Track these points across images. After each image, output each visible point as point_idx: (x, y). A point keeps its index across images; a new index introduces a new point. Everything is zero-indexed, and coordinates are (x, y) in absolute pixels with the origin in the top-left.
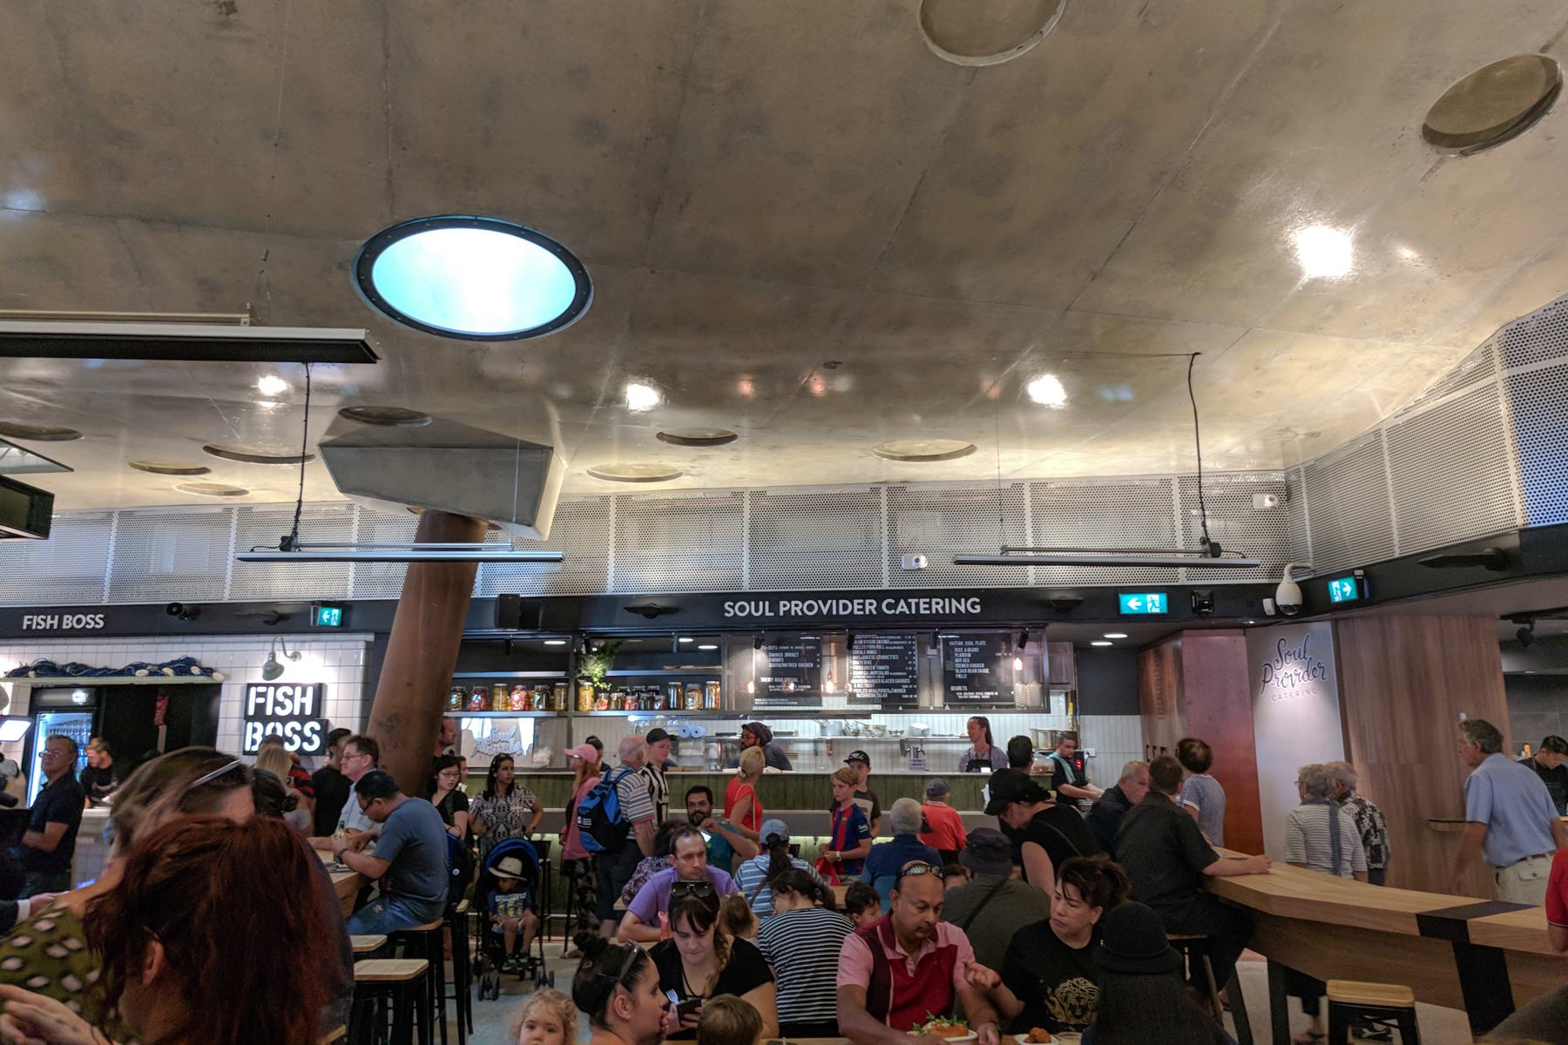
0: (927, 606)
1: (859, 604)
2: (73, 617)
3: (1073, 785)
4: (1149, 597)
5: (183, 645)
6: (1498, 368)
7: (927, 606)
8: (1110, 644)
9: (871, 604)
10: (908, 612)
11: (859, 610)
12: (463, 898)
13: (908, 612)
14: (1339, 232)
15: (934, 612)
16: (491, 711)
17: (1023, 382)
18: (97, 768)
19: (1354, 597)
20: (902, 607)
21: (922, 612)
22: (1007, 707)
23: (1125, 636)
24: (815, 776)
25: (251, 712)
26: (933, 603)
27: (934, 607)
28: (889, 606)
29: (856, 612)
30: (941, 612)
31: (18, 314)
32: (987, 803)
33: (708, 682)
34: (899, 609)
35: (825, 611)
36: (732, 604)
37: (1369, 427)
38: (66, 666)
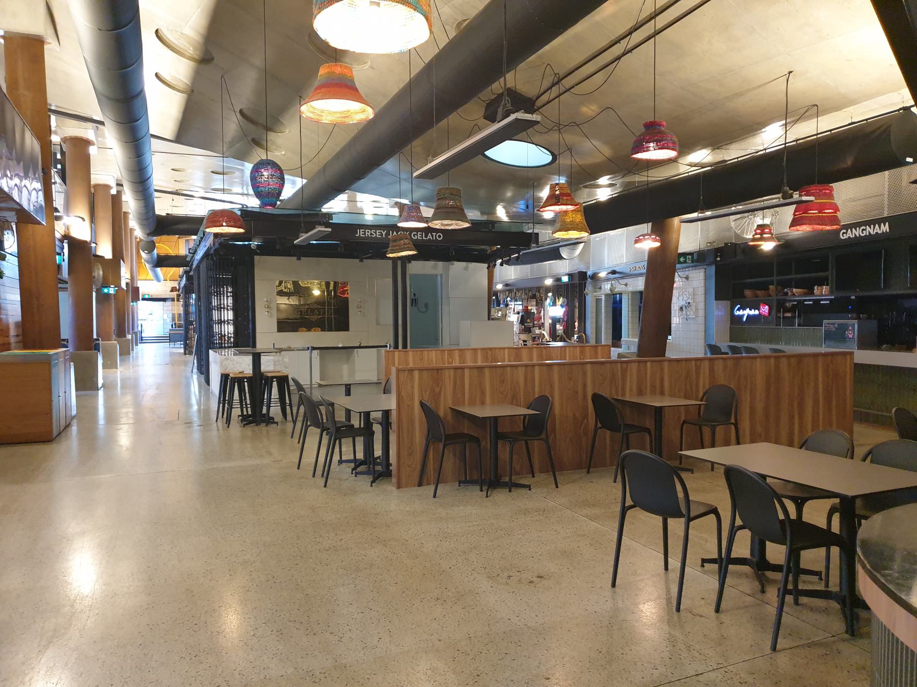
1: (362, 231)
8: (828, 302)
10: (432, 239)
11: (362, 234)
13: (432, 239)
14: (207, 211)
15: (367, 236)
18: (448, 171)
21: (361, 235)
23: (415, 253)
24: (462, 163)
27: (367, 233)
29: (378, 236)
30: (370, 236)
31: (768, 199)
32: (44, 206)
34: (428, 237)
35: (395, 233)
38: (207, 274)
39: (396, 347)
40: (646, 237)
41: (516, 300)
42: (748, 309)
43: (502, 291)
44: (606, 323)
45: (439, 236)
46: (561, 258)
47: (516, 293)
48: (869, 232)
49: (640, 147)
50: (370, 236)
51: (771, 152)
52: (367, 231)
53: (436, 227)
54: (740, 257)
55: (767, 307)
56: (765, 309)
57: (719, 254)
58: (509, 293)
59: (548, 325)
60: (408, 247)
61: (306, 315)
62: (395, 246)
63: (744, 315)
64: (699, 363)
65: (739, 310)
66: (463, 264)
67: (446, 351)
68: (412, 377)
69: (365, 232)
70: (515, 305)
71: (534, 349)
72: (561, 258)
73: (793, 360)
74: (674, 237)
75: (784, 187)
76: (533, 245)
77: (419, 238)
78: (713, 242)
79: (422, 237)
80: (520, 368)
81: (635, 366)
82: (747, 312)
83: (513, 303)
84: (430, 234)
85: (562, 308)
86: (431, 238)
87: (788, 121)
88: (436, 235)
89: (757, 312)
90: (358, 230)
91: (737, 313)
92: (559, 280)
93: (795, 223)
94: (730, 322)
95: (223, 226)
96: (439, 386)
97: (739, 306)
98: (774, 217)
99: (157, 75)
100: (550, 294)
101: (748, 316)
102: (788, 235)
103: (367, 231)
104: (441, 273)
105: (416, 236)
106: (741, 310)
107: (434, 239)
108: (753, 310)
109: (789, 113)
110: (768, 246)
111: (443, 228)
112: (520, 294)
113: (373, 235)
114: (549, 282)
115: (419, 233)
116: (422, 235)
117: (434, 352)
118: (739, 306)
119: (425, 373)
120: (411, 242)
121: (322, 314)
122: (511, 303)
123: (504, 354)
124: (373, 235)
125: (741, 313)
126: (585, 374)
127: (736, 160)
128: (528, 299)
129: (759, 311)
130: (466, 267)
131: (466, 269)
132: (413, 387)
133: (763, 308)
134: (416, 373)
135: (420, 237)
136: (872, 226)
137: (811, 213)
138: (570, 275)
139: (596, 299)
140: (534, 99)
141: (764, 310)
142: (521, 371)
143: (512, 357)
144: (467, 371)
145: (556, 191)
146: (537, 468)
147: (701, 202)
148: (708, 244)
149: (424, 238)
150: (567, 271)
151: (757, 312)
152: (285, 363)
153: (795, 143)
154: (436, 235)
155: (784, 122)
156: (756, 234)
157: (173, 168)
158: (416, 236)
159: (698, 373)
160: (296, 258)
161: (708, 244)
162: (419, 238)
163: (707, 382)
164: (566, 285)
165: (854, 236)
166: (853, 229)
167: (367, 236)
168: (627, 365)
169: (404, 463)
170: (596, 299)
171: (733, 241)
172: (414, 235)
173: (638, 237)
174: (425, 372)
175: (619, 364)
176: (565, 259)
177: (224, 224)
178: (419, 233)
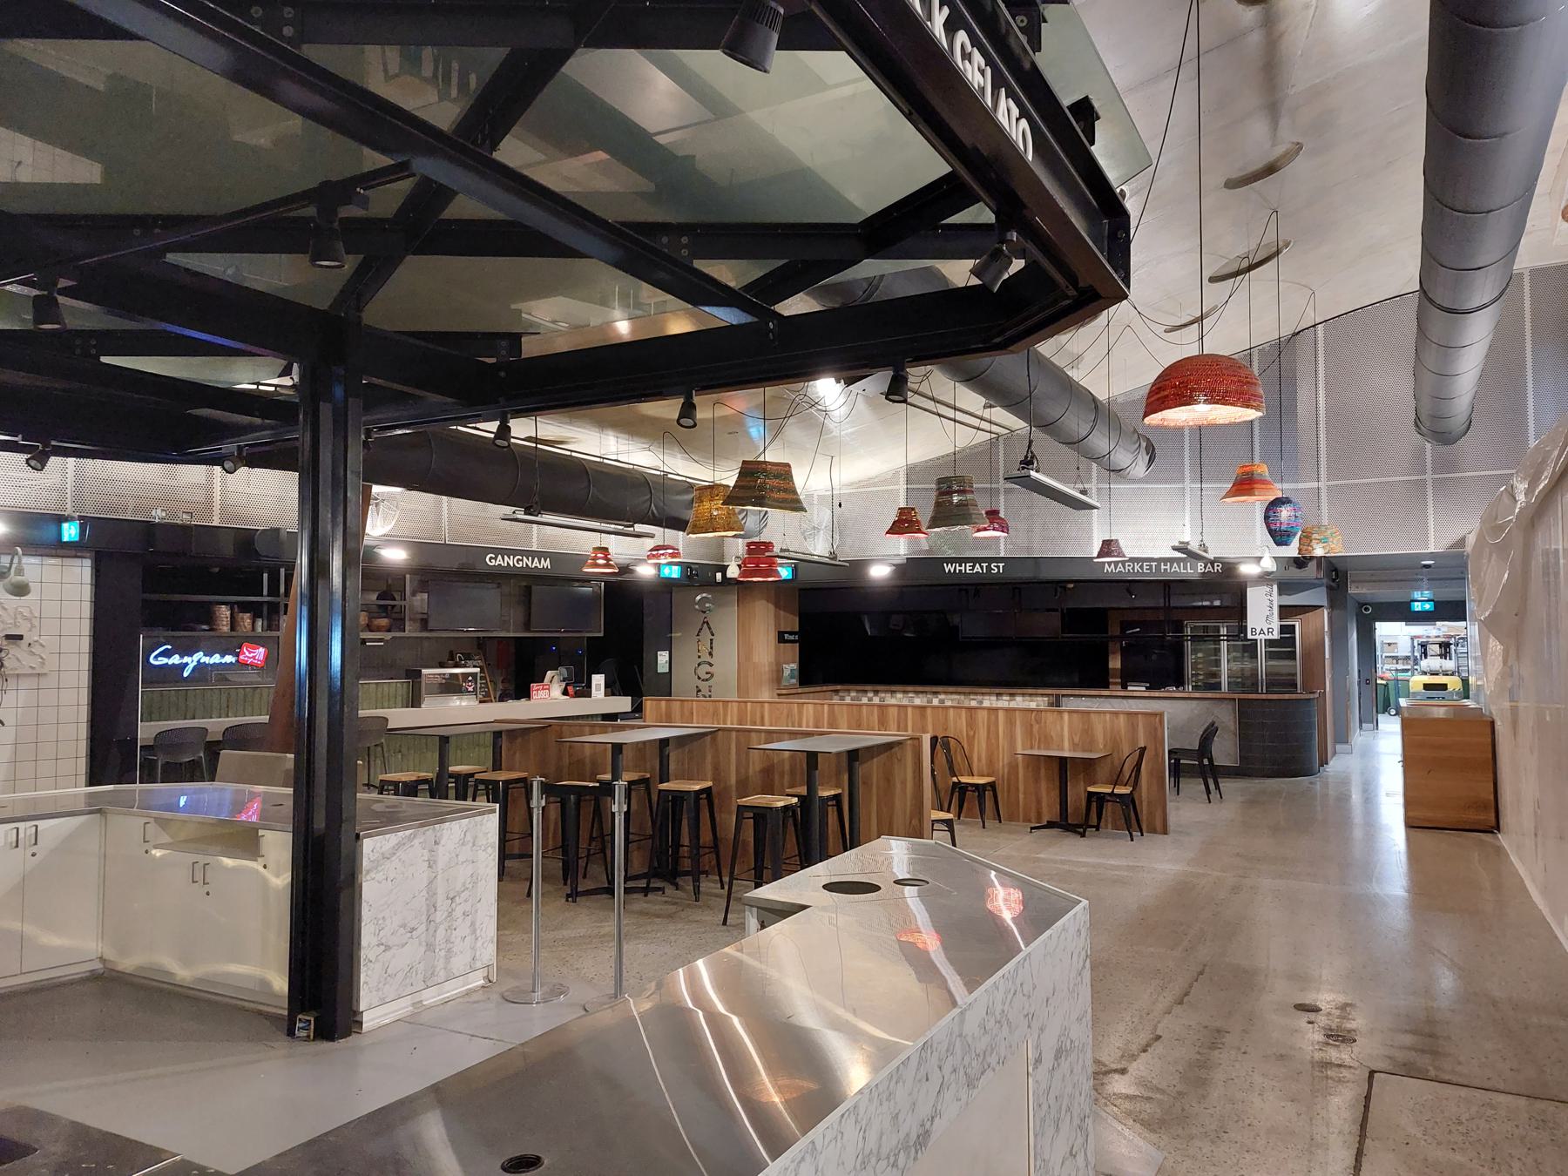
5: (76, 560)
6: (1429, 471)
9: (1218, 566)
16: (624, 893)
19: (77, 539)
20: (499, 561)
21: (968, 571)
22: (784, 501)
25: (988, 794)
27: (1216, 568)
33: (492, 436)
44: (1352, 647)
48: (527, 564)
51: (577, 458)
68: (1062, 718)
105: (520, 562)
106: (177, 656)
118: (169, 647)
127: (631, 467)
132: (1062, 728)
133: (250, 652)
135: (1147, 569)
136: (530, 558)
143: (1076, 735)
146: (1531, 724)
158: (520, 562)
165: (506, 565)
166: (536, 559)
174: (1075, 715)
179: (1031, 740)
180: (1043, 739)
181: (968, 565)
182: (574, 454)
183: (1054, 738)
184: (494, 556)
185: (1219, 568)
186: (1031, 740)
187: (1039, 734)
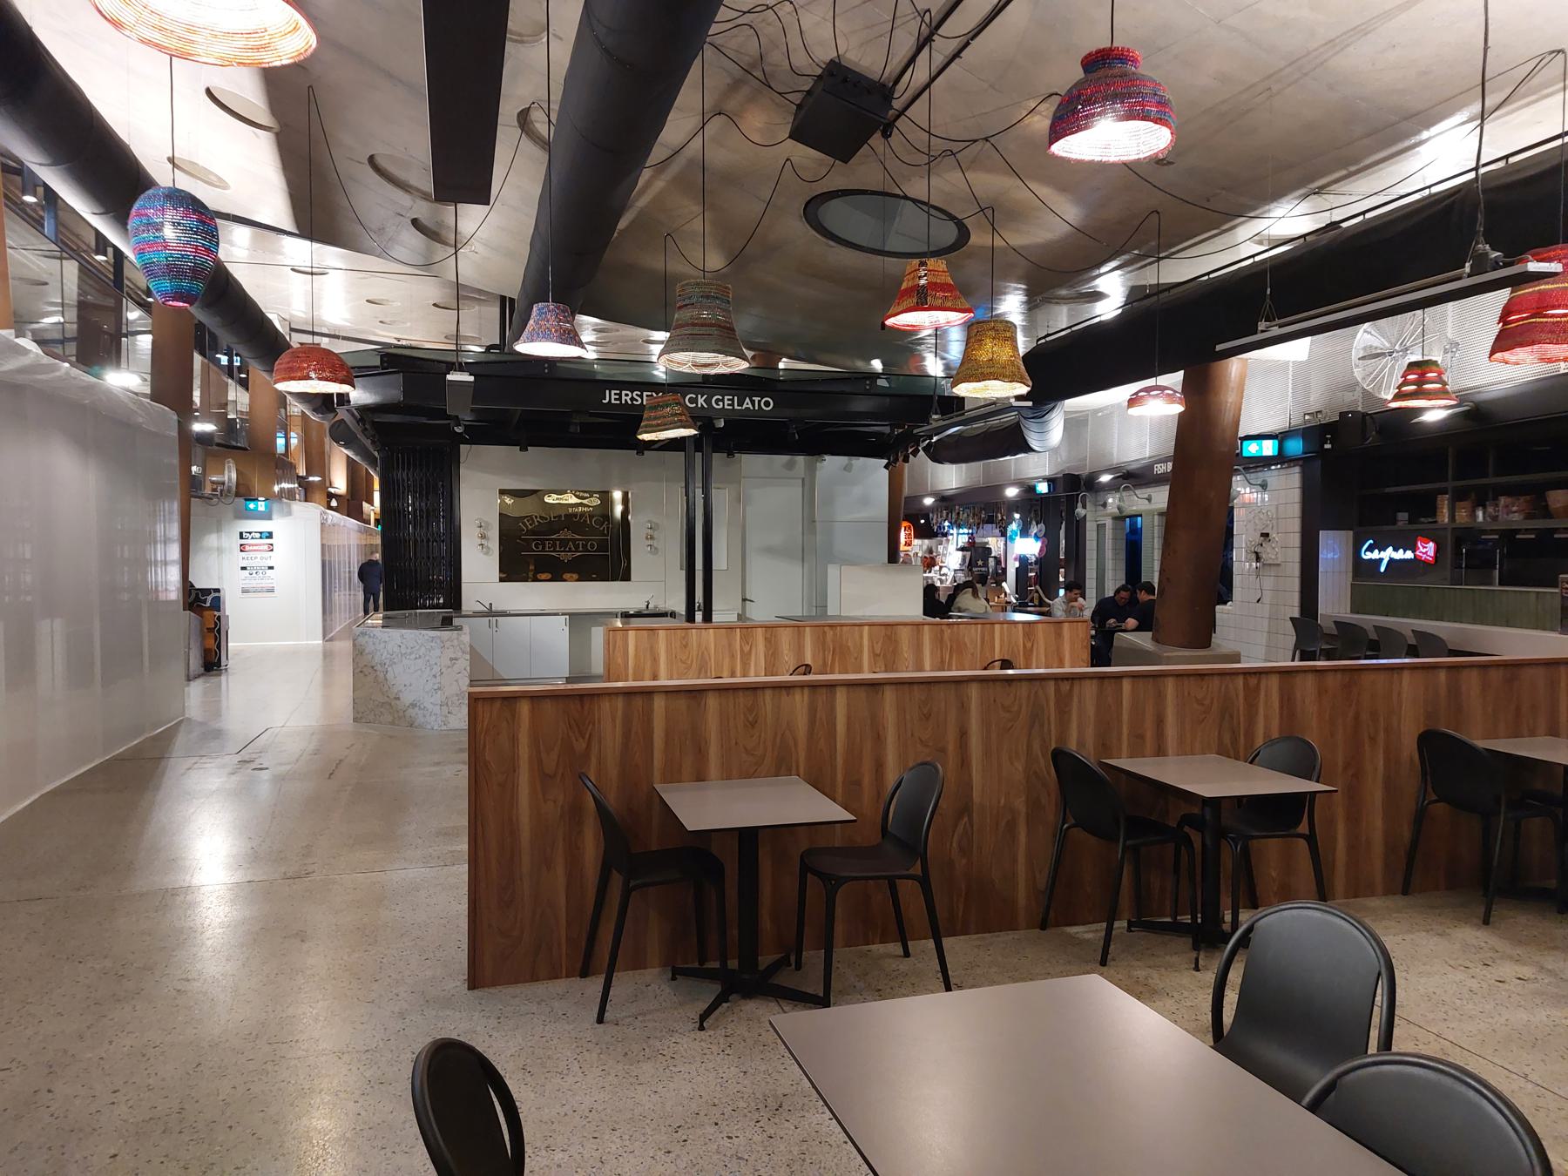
0: (617, 397)
1: (615, 394)
2: (762, 399)
3: (931, 671)
4: (324, 338)
7: (617, 397)
10: (752, 408)
11: (616, 399)
12: (1560, 261)
13: (752, 408)
15: (623, 402)
17: (1005, 294)
21: (613, 401)
26: (623, 395)
27: (624, 398)
28: (691, 400)
30: (630, 402)
34: (745, 406)
36: (639, 393)
37: (1110, 463)
39: (690, 617)
40: (1152, 393)
41: (959, 527)
42: (1391, 548)
43: (932, 509)
45: (767, 404)
46: (1027, 449)
47: (958, 514)
49: (1068, 119)
50: (630, 402)
52: (624, 392)
53: (681, 369)
54: (1372, 438)
55: (1431, 545)
56: (1428, 550)
57: (1329, 436)
58: (947, 514)
59: (1014, 571)
60: (681, 421)
61: (551, 551)
62: (655, 418)
63: (1381, 560)
64: (1253, 681)
65: (1370, 549)
66: (841, 460)
67: (738, 630)
69: (620, 395)
70: (958, 534)
71: (926, 627)
72: (1027, 449)
73: (1496, 676)
74: (1230, 400)
75: (1477, 243)
76: (935, 417)
77: (726, 407)
78: (1317, 412)
79: (733, 405)
80: (798, 692)
81: (1090, 689)
82: (1388, 554)
83: (954, 531)
84: (748, 400)
85: (1037, 541)
86: (750, 406)
87: (1490, 102)
88: (759, 402)
89: (1409, 555)
90: (607, 392)
91: (1368, 556)
92: (1032, 489)
93: (1505, 341)
94: (1351, 574)
95: (311, 378)
96: (583, 738)
97: (1371, 541)
98: (1449, 355)
99: (209, 92)
100: (1017, 516)
101: (1391, 560)
102: (1479, 392)
103: (624, 392)
104: (803, 476)
105: (721, 403)
107: (757, 408)
108: (1401, 551)
109: (1488, 80)
110: (1435, 413)
111: (697, 371)
112: (965, 515)
113: (637, 401)
114: (1012, 492)
115: (726, 398)
116: (733, 400)
117: (711, 631)
118: (1371, 541)
119: (548, 706)
120: (686, 413)
121: (581, 549)
122: (951, 531)
123: (861, 637)
124: (637, 401)
125: (1375, 555)
126: (963, 708)
127: (1360, 218)
128: (979, 524)
129: (1414, 551)
130: (847, 465)
131: (847, 468)
132: (514, 740)
133: (1424, 547)
134: (524, 708)
137: (1553, 316)
138: (1051, 481)
139: (1098, 525)
140: (891, 84)
141: (1424, 551)
142: (800, 700)
143: (877, 643)
144: (659, 703)
145: (920, 278)
147: (1268, 300)
148: (1307, 417)
149: (736, 407)
150: (1047, 472)
151: (1409, 555)
152: (464, 644)
153: (1501, 164)
154: (759, 402)
155: (1476, 108)
156: (1405, 383)
157: (369, 298)
158: (721, 403)
159: (1251, 707)
160: (518, 447)
161: (1307, 417)
162: (726, 407)
163: (1275, 723)
164: (1043, 497)
167: (623, 402)
168: (1072, 686)
169: (995, 701)
170: (1098, 525)
171: (1360, 409)
172: (717, 401)
173: (1136, 394)
175: (1052, 683)
176: (1034, 451)
177: (313, 375)
178: (726, 398)
179: (824, 651)
180: (955, 647)
181: (613, 392)
182: (1368, 216)
183: (852, 649)
184: (721, 398)
185: (628, 398)
186: (824, 651)
187: (951, 641)
